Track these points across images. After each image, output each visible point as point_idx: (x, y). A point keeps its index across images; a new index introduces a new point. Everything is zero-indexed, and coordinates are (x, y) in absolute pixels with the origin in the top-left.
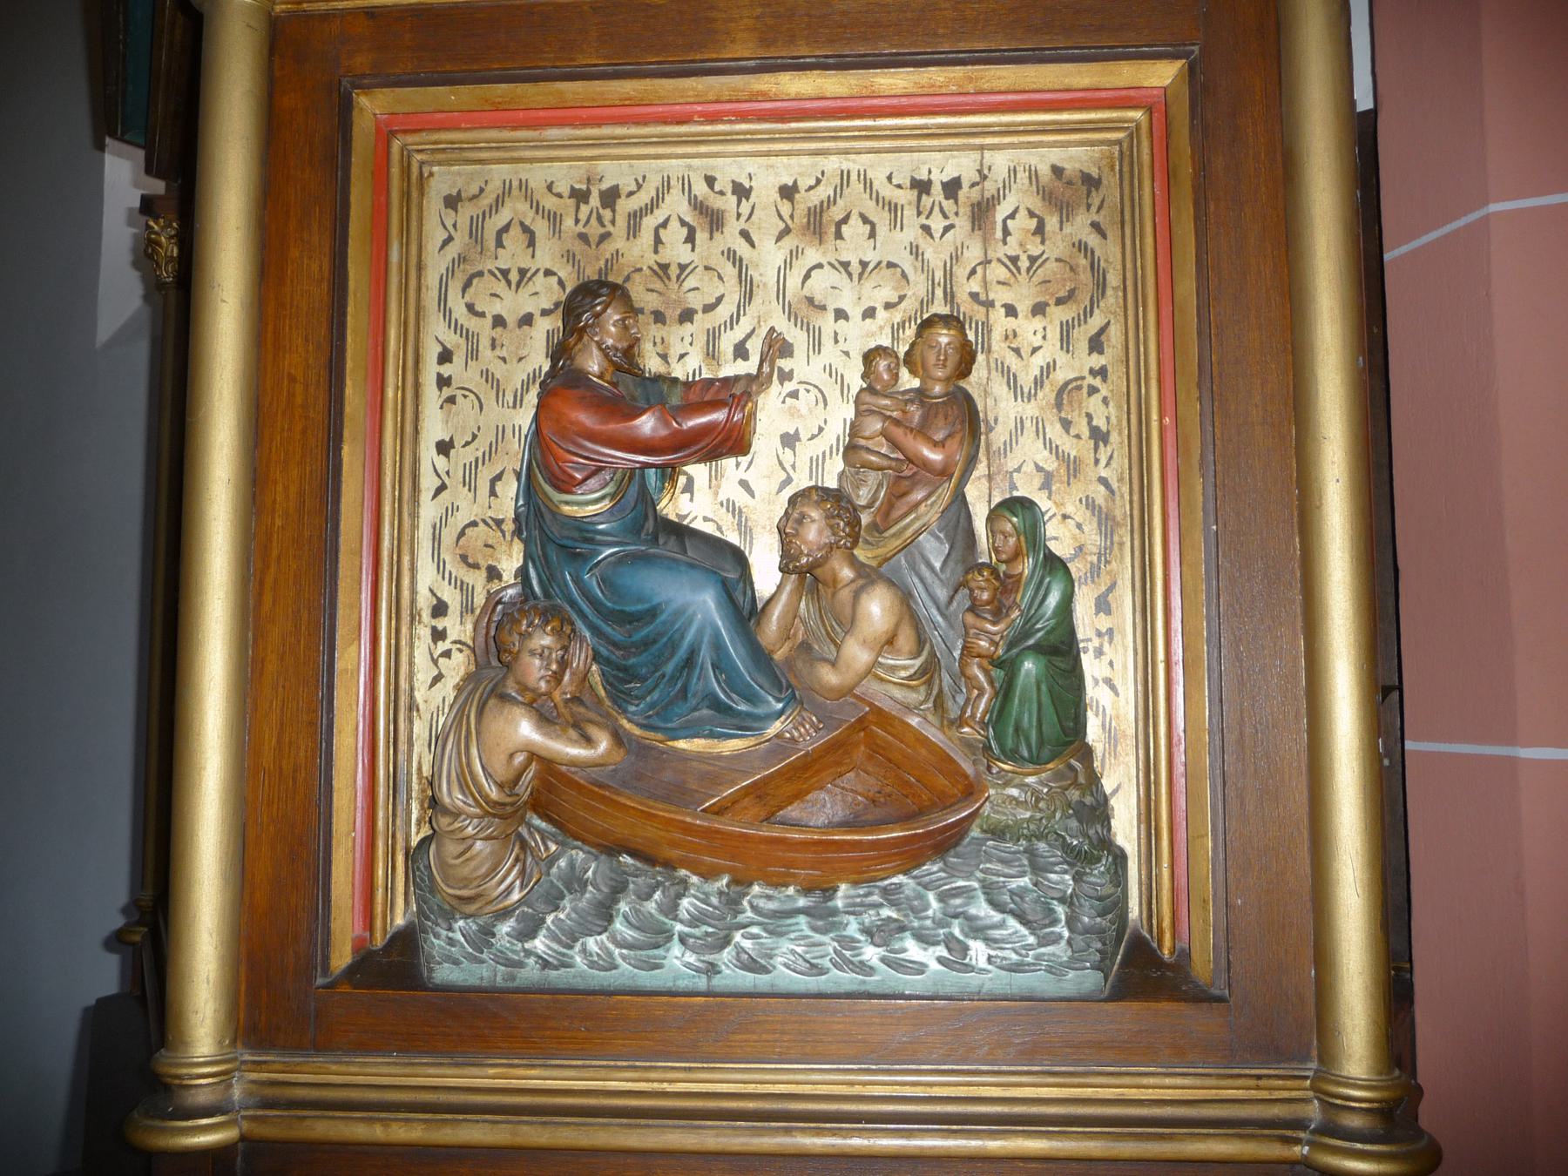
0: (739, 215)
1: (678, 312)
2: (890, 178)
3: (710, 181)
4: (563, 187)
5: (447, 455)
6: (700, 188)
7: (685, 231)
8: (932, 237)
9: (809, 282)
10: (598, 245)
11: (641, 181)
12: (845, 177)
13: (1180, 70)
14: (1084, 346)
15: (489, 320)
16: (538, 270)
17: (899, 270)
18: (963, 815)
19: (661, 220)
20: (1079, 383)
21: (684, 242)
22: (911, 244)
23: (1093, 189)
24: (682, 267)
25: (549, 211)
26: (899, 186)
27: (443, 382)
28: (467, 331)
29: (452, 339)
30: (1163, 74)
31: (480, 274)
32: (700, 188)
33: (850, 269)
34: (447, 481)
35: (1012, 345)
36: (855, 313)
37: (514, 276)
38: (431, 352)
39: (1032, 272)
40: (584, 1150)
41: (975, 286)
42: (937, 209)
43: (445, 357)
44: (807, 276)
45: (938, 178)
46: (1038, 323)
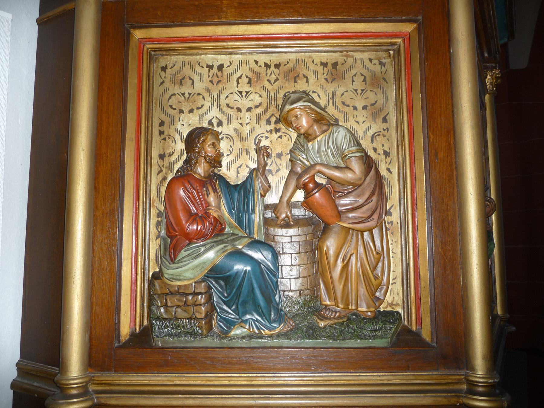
0: (267, 74)
1: (240, 107)
2: (313, 62)
3: (256, 62)
4: (317, 61)
5: (163, 160)
6: (253, 65)
7: (247, 80)
8: (213, 85)
9: (170, 100)
10: (217, 84)
11: (232, 62)
12: (184, 63)
13: (415, 28)
14: (381, 120)
15: (178, 111)
16: (195, 94)
17: (201, 96)
18: (461, 279)
19: (239, 76)
20: (379, 133)
21: (247, 84)
22: (206, 87)
23: (268, 68)
24: (247, 93)
25: (372, 70)
26: (316, 64)
27: (161, 133)
28: (170, 115)
29: (164, 117)
30: (408, 28)
31: (174, 95)
32: (253, 65)
33: (357, 92)
34: (280, 167)
35: (356, 120)
36: (186, 110)
37: (244, 94)
38: (156, 122)
39: (362, 94)
40: (193, 407)
41: (227, 101)
42: (273, 72)
43: (162, 124)
44: (170, 98)
45: (216, 64)
46: (248, 115)
